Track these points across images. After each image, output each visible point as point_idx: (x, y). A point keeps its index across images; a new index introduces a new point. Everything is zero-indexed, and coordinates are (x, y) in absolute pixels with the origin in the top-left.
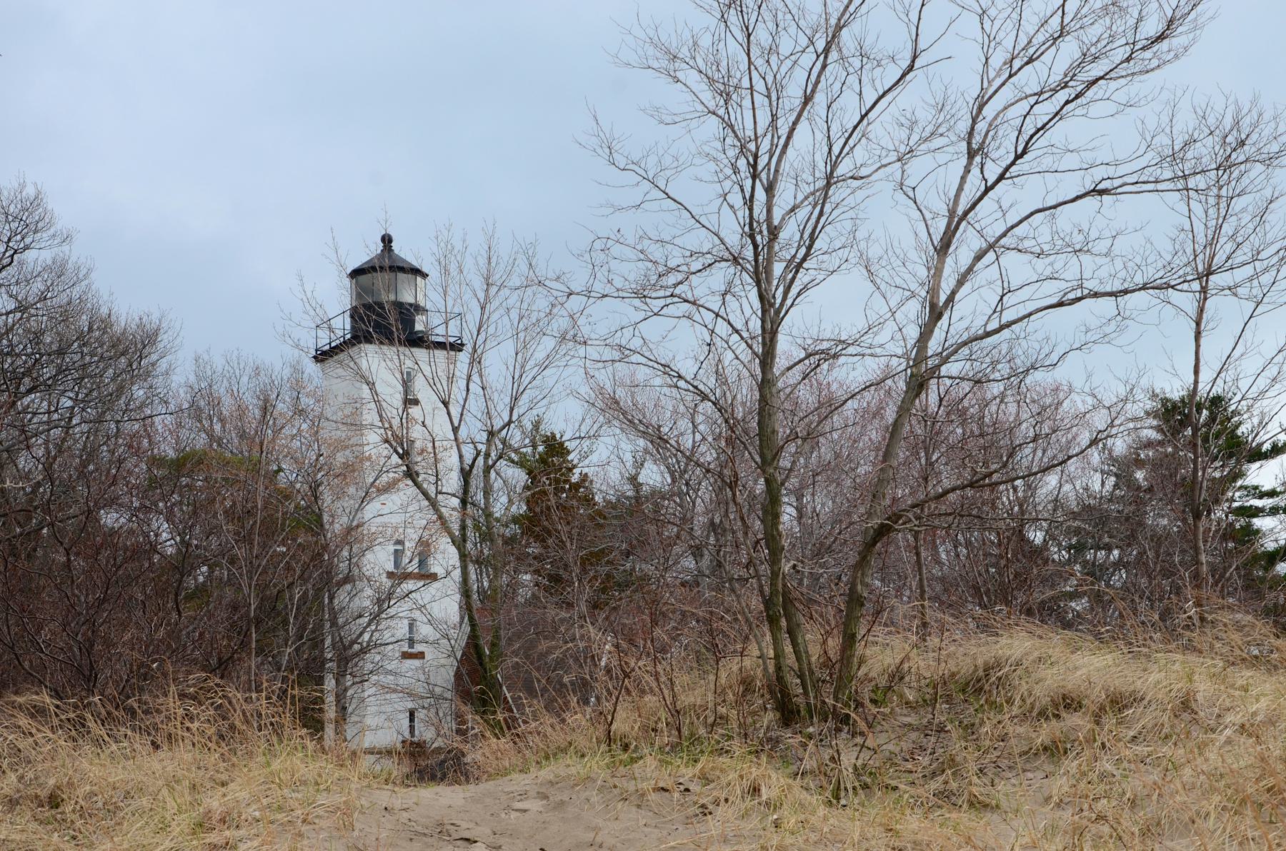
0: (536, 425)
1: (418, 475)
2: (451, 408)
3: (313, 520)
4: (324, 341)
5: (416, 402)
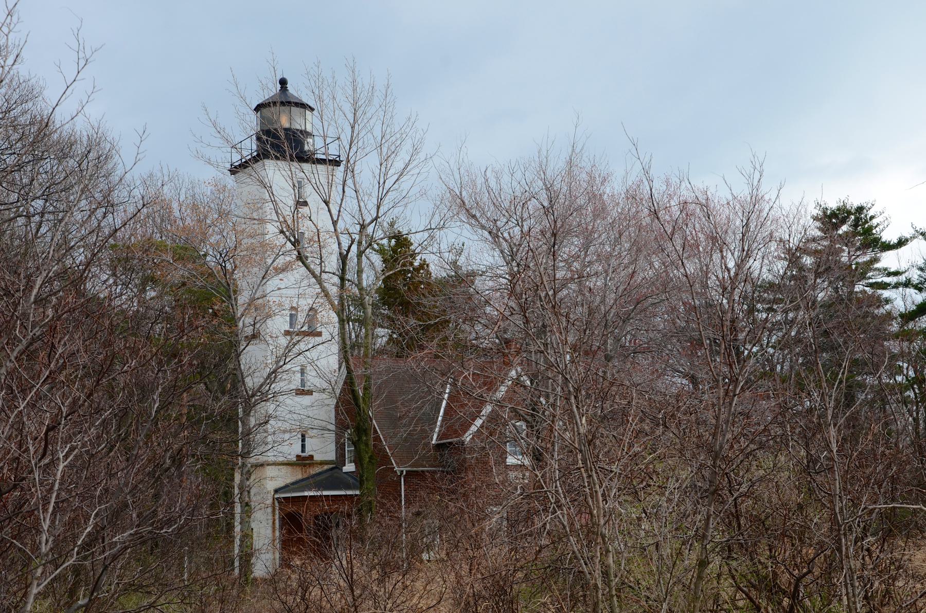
0: (392, 225)
1: (307, 257)
2: (331, 205)
3: (229, 291)
4: (236, 159)
5: (305, 204)
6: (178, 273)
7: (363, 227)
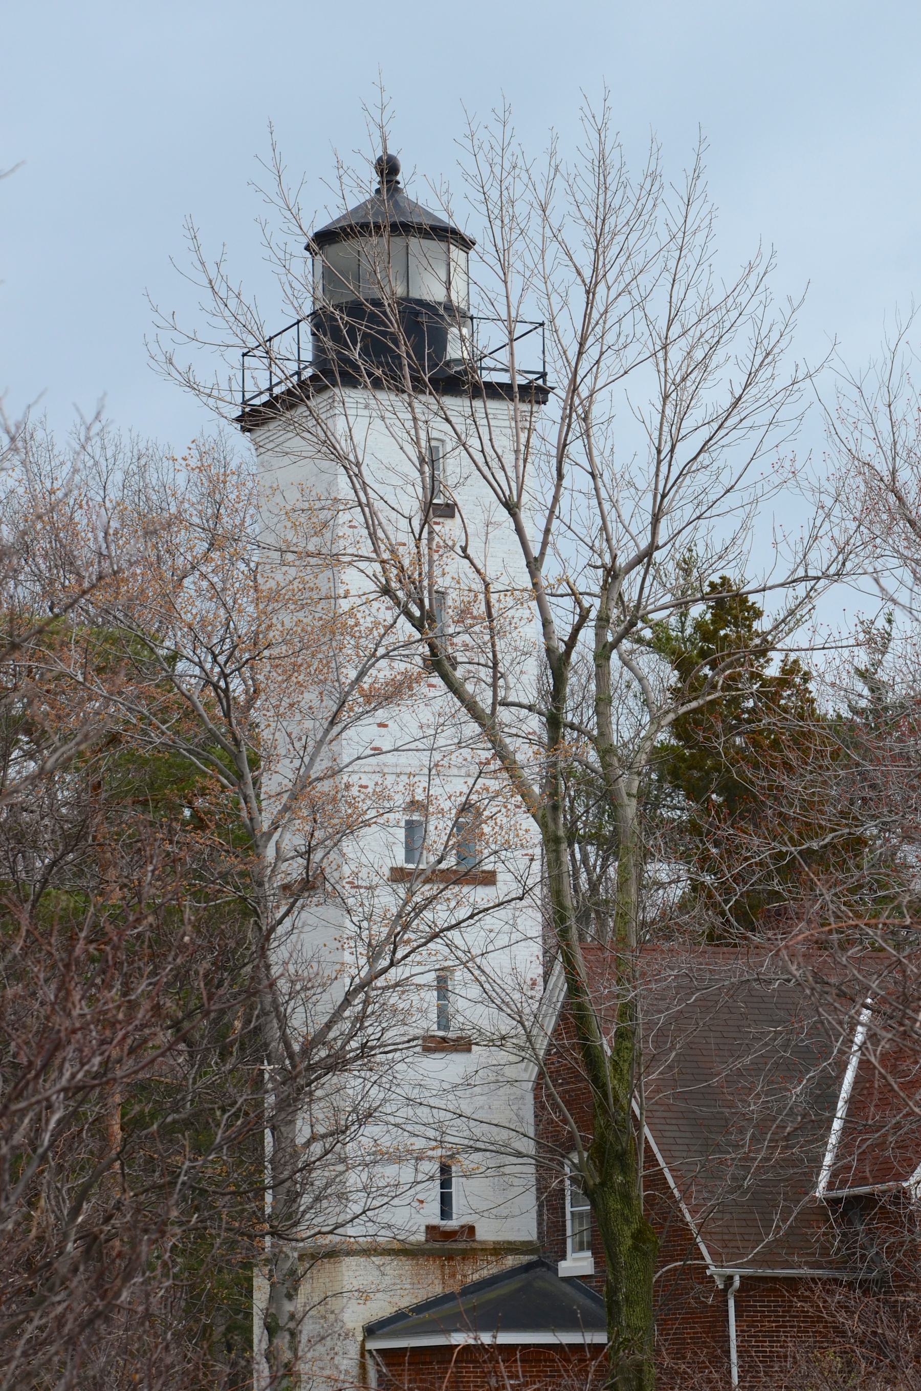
1: (455, 664)
2: (523, 516)
3: (240, 761)
4: (259, 381)
5: (449, 510)
6: (103, 706)
7: (612, 574)
